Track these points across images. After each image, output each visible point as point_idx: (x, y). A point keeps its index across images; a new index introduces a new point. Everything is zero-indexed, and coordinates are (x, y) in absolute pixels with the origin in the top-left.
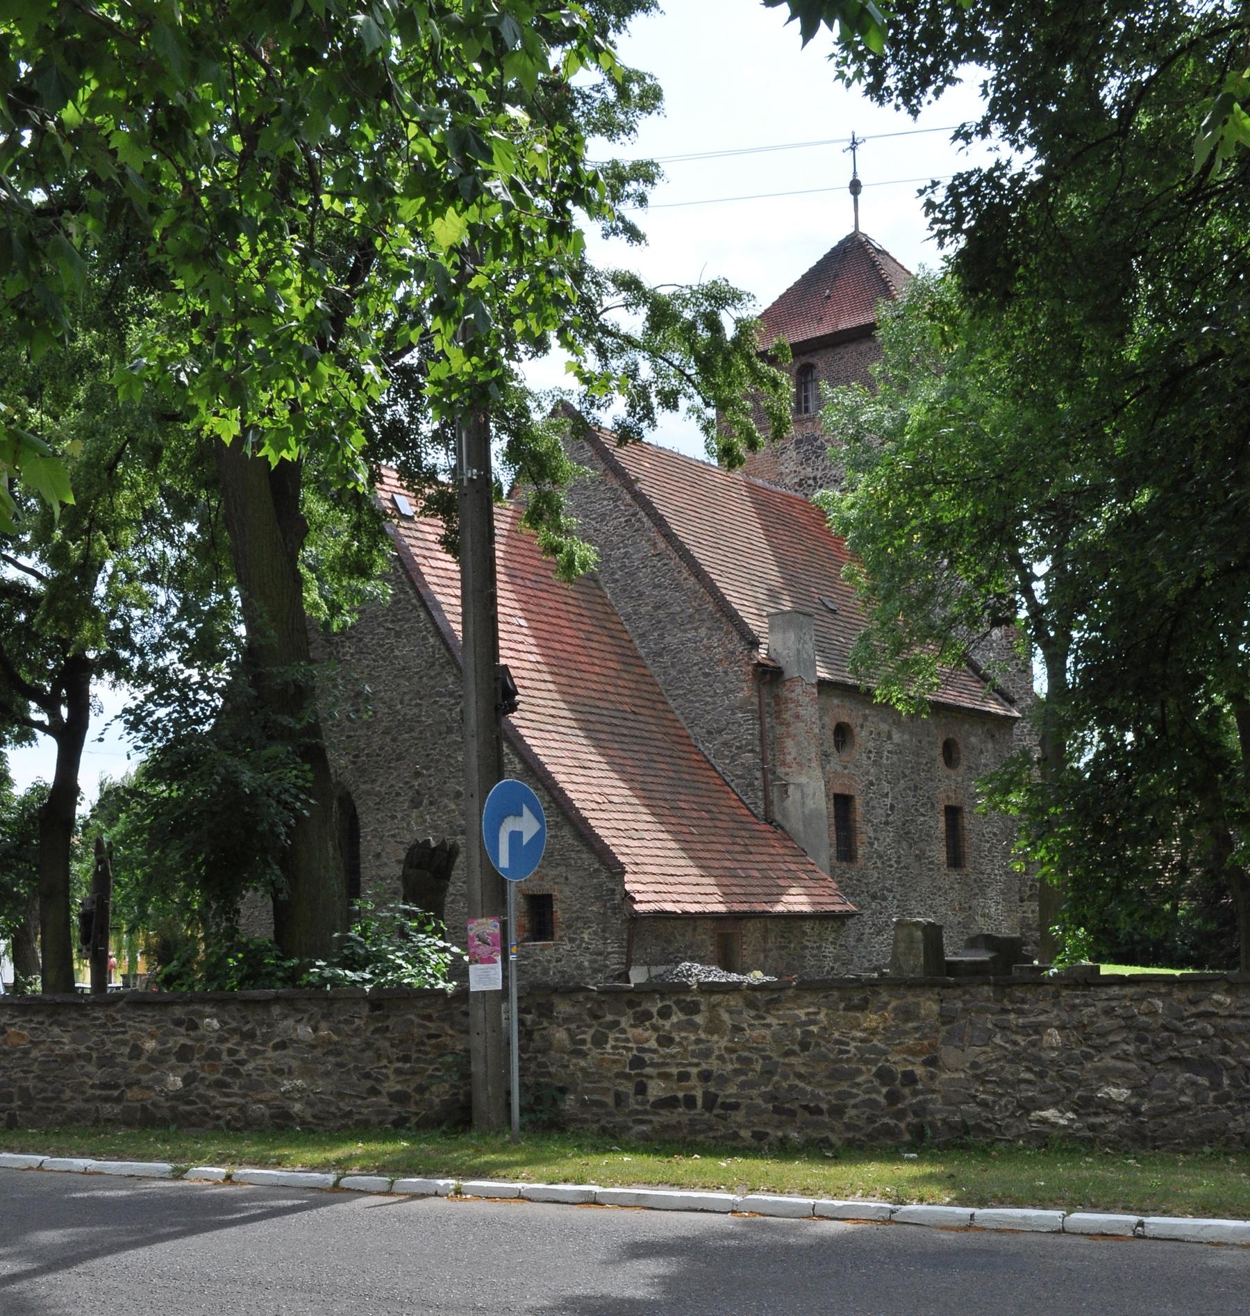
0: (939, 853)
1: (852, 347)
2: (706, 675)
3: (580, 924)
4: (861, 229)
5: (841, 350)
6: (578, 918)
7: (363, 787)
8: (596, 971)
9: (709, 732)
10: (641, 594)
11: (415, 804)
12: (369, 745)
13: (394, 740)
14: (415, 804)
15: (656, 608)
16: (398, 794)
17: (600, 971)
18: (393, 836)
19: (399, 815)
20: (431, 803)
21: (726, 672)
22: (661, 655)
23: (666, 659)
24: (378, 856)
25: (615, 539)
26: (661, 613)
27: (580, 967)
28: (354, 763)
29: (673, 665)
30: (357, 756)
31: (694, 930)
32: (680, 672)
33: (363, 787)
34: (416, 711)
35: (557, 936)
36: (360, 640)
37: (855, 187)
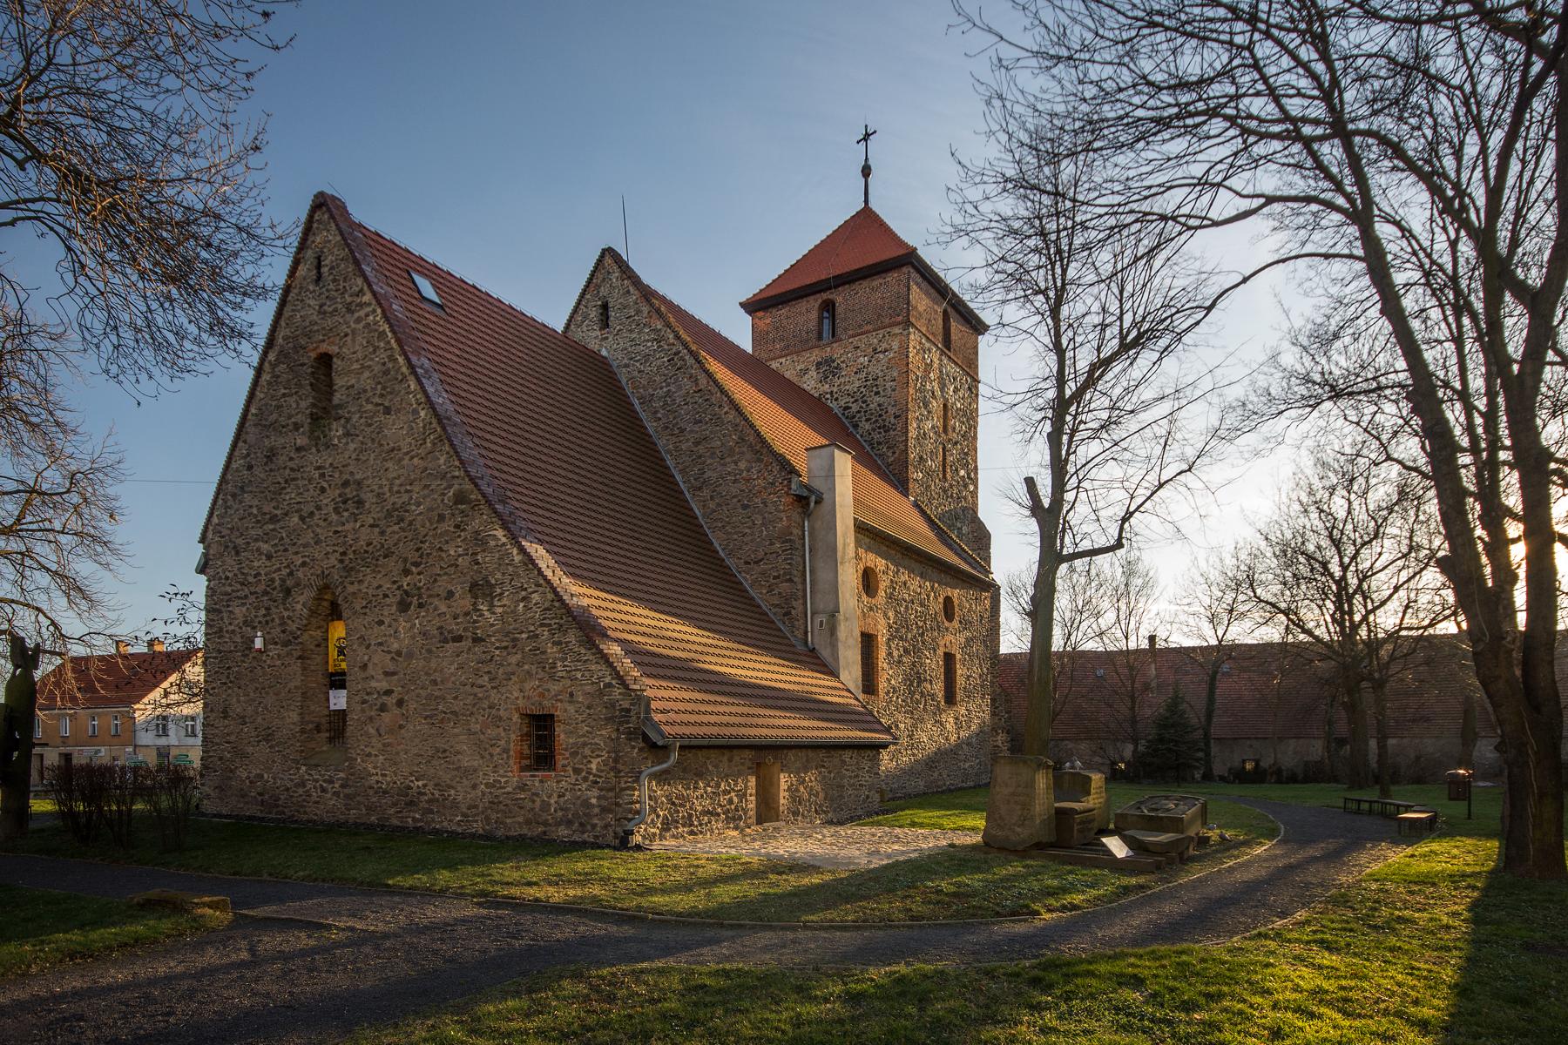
0: (938, 688)
1: (865, 283)
2: (745, 507)
3: (587, 751)
4: (873, 205)
5: (856, 286)
6: (585, 744)
7: (351, 589)
8: (604, 810)
9: (747, 563)
10: (682, 430)
11: (404, 606)
12: (356, 540)
13: (382, 533)
14: (404, 606)
15: (697, 443)
16: (386, 596)
17: (610, 811)
18: (380, 644)
19: (387, 621)
20: (421, 606)
21: (764, 503)
22: (700, 489)
23: (706, 493)
24: (364, 667)
25: (658, 378)
26: (701, 449)
27: (586, 803)
28: (341, 561)
29: (712, 498)
30: (344, 554)
31: (730, 760)
32: (719, 505)
33: (351, 589)
34: (405, 498)
35: (559, 766)
36: (348, 420)
37: (866, 171)
